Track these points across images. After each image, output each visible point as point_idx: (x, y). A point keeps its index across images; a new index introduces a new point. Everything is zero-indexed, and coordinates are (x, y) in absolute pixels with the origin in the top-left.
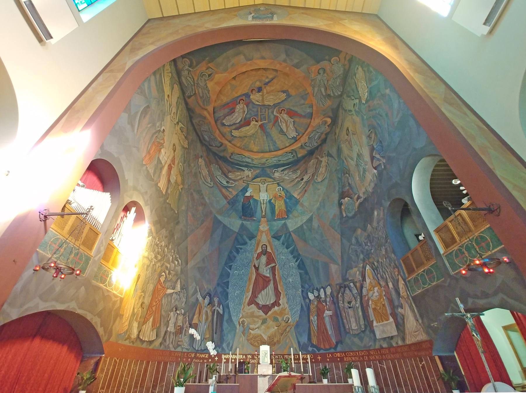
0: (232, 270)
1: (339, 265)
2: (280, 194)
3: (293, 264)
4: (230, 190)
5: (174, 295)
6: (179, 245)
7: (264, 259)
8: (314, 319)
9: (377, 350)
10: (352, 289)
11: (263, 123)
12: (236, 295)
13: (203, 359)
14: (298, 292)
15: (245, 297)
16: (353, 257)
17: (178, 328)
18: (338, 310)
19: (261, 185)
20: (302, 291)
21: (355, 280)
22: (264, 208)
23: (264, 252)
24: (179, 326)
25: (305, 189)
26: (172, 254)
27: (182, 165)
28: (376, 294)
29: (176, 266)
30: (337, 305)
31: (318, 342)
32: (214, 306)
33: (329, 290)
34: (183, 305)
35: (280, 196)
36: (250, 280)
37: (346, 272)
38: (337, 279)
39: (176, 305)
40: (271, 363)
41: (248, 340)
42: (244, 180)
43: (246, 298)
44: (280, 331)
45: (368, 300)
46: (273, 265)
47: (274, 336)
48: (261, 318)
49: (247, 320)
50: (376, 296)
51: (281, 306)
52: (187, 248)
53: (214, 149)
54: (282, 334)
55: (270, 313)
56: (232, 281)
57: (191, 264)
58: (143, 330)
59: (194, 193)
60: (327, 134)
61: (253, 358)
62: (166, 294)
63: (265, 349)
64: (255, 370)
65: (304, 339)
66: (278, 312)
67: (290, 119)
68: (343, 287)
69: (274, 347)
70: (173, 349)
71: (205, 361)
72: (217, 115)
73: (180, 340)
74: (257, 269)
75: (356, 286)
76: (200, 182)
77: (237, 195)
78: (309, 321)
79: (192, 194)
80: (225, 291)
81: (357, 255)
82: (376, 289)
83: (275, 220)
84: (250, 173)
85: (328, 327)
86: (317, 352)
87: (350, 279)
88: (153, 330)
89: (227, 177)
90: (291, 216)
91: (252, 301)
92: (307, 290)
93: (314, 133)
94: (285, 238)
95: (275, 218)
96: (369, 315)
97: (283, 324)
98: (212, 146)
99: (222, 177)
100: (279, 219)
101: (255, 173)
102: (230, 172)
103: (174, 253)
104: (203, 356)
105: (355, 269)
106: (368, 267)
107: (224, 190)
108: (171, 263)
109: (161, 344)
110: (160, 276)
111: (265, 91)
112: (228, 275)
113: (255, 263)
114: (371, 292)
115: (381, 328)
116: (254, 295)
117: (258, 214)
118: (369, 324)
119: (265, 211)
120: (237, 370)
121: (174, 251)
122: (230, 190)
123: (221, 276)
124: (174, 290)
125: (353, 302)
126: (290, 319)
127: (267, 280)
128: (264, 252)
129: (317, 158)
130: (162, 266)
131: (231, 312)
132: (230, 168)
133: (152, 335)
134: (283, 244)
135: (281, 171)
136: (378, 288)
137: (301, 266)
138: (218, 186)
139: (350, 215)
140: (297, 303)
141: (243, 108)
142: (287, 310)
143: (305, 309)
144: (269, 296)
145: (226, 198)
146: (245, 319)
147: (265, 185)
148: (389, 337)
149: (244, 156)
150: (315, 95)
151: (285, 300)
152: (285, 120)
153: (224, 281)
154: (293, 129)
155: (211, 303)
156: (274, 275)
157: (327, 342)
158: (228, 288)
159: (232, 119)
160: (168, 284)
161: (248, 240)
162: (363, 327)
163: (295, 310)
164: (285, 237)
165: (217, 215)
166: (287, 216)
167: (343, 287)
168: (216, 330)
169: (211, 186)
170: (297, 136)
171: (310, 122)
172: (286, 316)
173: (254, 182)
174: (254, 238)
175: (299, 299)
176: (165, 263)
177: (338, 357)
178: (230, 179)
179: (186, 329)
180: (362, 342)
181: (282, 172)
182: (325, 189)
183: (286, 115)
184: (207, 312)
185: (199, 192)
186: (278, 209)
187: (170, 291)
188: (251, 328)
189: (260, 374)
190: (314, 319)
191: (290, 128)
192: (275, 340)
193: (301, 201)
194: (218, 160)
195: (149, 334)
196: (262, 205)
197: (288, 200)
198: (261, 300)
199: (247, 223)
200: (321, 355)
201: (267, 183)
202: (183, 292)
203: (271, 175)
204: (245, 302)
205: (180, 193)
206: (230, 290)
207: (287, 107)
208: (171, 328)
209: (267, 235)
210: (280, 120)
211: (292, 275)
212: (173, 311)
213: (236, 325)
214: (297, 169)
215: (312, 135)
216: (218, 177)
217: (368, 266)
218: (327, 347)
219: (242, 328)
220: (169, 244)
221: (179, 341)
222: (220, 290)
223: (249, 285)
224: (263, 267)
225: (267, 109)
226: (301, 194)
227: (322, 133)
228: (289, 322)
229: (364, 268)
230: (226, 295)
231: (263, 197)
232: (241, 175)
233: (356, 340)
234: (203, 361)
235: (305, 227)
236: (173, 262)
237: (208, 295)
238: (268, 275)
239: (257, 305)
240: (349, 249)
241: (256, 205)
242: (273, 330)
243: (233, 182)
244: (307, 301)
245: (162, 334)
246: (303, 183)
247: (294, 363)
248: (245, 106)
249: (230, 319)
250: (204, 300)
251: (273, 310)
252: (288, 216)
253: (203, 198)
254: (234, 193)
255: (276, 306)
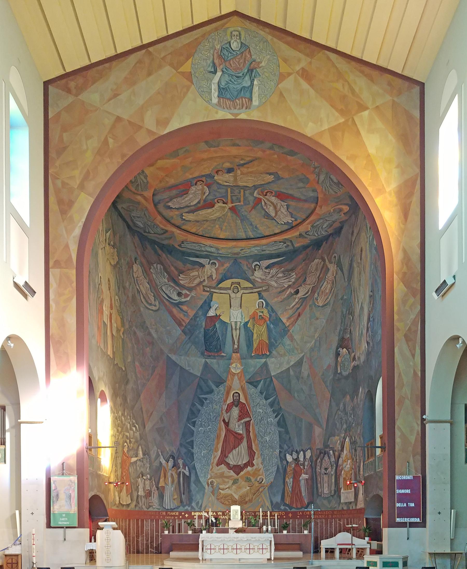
0: (196, 426)
1: (323, 429)
2: (262, 314)
3: (272, 420)
4: (185, 308)
5: (138, 463)
6: (133, 407)
7: (235, 411)
8: (289, 481)
9: (339, 511)
10: (331, 457)
11: (235, 205)
12: (202, 455)
13: (174, 516)
14: (275, 453)
15: (213, 456)
16: (338, 424)
17: (147, 492)
18: (315, 475)
19: (233, 295)
20: (280, 452)
21: (335, 449)
22: (236, 336)
23: (236, 403)
24: (147, 490)
25: (299, 311)
26: (129, 420)
27: (118, 299)
28: (348, 466)
29: (134, 433)
30: (314, 470)
31: (291, 502)
32: (179, 468)
33: (308, 454)
34: (148, 470)
35: (262, 318)
36: (218, 437)
37: (329, 439)
38: (319, 445)
39: (142, 472)
40: (242, 519)
41: (218, 499)
42: (206, 286)
43: (214, 458)
44: (253, 491)
45: (342, 469)
46: (248, 419)
47: (246, 496)
48: (232, 478)
49: (216, 480)
50: (348, 468)
51: (254, 467)
52: (142, 408)
53: (152, 236)
54: (254, 494)
55: (242, 473)
56: (197, 440)
57: (149, 426)
58: (121, 497)
59: (136, 331)
60: (343, 223)
61: (224, 514)
62: (131, 463)
63: (236, 509)
64: (227, 524)
65: (278, 499)
66: (251, 473)
67: (281, 202)
68: (323, 453)
69: (245, 506)
70: (146, 510)
71: (176, 518)
72: (157, 198)
73: (150, 501)
74: (227, 424)
75: (334, 454)
76: (142, 309)
77: (195, 316)
78: (284, 482)
79: (135, 333)
80: (189, 451)
81: (341, 423)
82: (349, 461)
83: (252, 357)
84: (214, 270)
85: (303, 489)
86: (289, 510)
87: (331, 447)
88: (127, 496)
89: (176, 283)
90: (274, 352)
91: (222, 461)
92: (285, 451)
93: (322, 221)
94: (265, 385)
95: (253, 355)
96: (339, 482)
97: (257, 484)
98: (149, 233)
99: (170, 286)
100: (259, 356)
101: (221, 270)
102: (181, 272)
103: (130, 419)
104: (174, 514)
105: (337, 438)
106: (347, 440)
107: (175, 311)
108: (130, 431)
109: (136, 506)
110: (123, 447)
111: (239, 172)
112: (192, 433)
113: (224, 417)
114: (345, 463)
115: (346, 494)
116: (224, 455)
117: (228, 348)
118: (338, 490)
119: (238, 342)
120: (210, 524)
121: (130, 417)
122: (185, 308)
123: (184, 435)
124: (137, 457)
125: (329, 470)
126: (264, 480)
127: (240, 437)
128: (236, 403)
129: (324, 260)
130: (123, 437)
131: (199, 474)
132: (180, 264)
133: (128, 499)
134: (261, 393)
135: (266, 268)
136: (351, 462)
137: (282, 423)
138: (165, 306)
139: (345, 373)
140: (273, 464)
141: (203, 190)
142: (261, 471)
143: (281, 471)
144: (241, 455)
145: (180, 324)
146: (213, 480)
147: (239, 295)
148: (349, 502)
149: (202, 245)
150: (320, 182)
151: (260, 460)
152: (272, 203)
153: (187, 441)
154: (286, 213)
155: (175, 465)
156: (248, 431)
157: (299, 502)
158: (193, 448)
159: (183, 201)
160: (131, 453)
161: (214, 387)
162: (333, 492)
163: (271, 471)
164: (265, 383)
165: (170, 355)
166: (269, 351)
167: (323, 453)
168: (184, 491)
169: (157, 308)
170: (293, 221)
171: (315, 208)
172: (260, 477)
173: (221, 289)
174: (223, 383)
175: (276, 460)
176: (125, 433)
177: (307, 515)
178: (183, 287)
179: (154, 492)
180: (329, 503)
181: (267, 271)
182: (325, 321)
183: (274, 198)
184: (172, 475)
185: (143, 326)
186: (256, 339)
187: (134, 459)
188: (221, 488)
189: (231, 527)
190: (289, 481)
191: (282, 212)
192: (247, 499)
193: (291, 331)
194: (160, 252)
195: (126, 500)
196: (234, 331)
197: (272, 326)
198: (232, 459)
199: (213, 362)
200: (292, 513)
201: (242, 291)
202: (145, 457)
203: (249, 273)
204: (213, 463)
205: (123, 340)
206: (195, 450)
207: (275, 189)
208: (141, 493)
209: (240, 379)
210: (265, 202)
211: (270, 433)
212: (140, 477)
213: (205, 486)
214: (292, 270)
215: (318, 223)
216: (164, 288)
217: (347, 438)
218: (299, 506)
219: (211, 488)
220: (124, 411)
221: (150, 503)
222: (183, 450)
223: (218, 443)
224: (235, 422)
225: (242, 191)
226: (292, 319)
227: (334, 222)
228: (262, 483)
229: (345, 439)
230: (191, 455)
231: (236, 317)
232: (199, 276)
233: (325, 502)
234: (174, 518)
235: (292, 373)
236: (131, 429)
237: (171, 457)
238: (241, 432)
239: (228, 465)
240: (336, 415)
241: (224, 332)
242: (246, 490)
243: (188, 293)
244: (285, 462)
245: (135, 498)
246: (297, 300)
247: (262, 519)
248: (205, 187)
249: (198, 480)
250: (168, 462)
251: (245, 471)
252: (270, 352)
253: (149, 334)
254: (191, 313)
255: (249, 467)
